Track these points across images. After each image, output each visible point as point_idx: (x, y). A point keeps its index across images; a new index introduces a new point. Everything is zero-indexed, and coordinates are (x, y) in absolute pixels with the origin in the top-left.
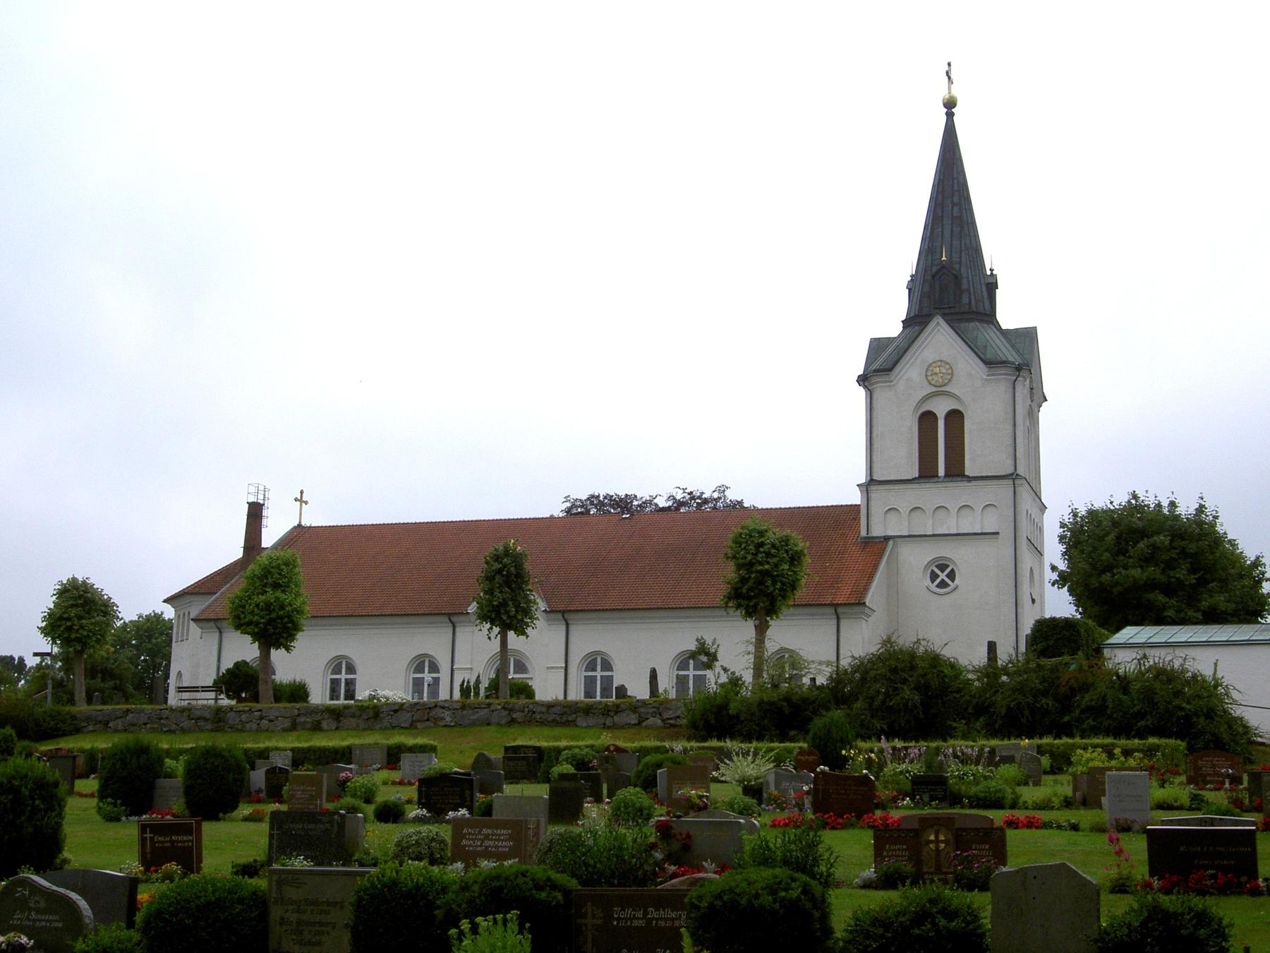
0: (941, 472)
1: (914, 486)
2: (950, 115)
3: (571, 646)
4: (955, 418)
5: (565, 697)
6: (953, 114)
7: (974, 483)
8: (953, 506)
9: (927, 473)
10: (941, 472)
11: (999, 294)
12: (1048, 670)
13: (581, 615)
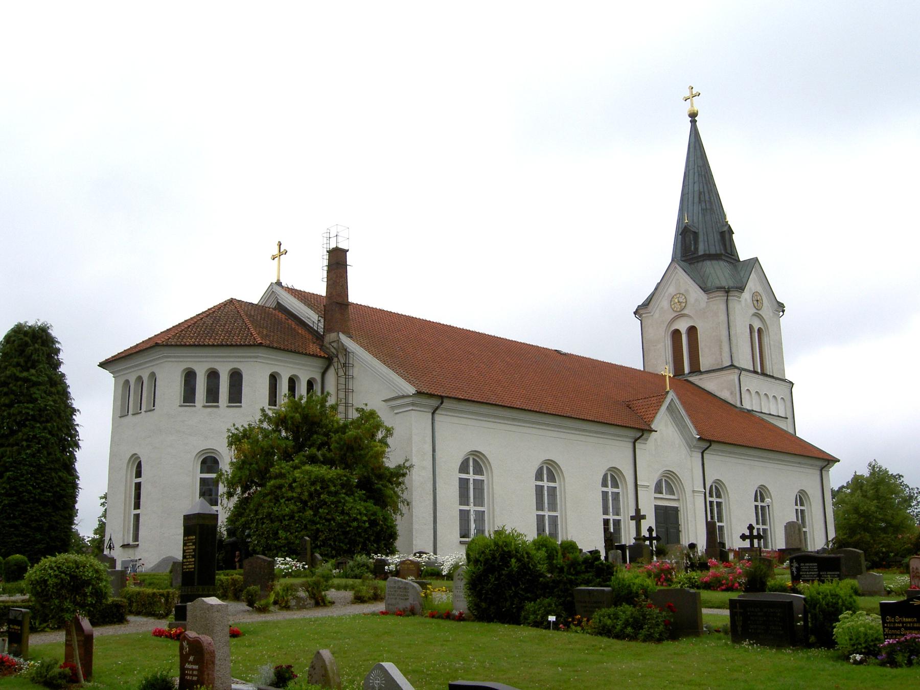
0: (687, 370)
2: (694, 122)
4: (692, 331)
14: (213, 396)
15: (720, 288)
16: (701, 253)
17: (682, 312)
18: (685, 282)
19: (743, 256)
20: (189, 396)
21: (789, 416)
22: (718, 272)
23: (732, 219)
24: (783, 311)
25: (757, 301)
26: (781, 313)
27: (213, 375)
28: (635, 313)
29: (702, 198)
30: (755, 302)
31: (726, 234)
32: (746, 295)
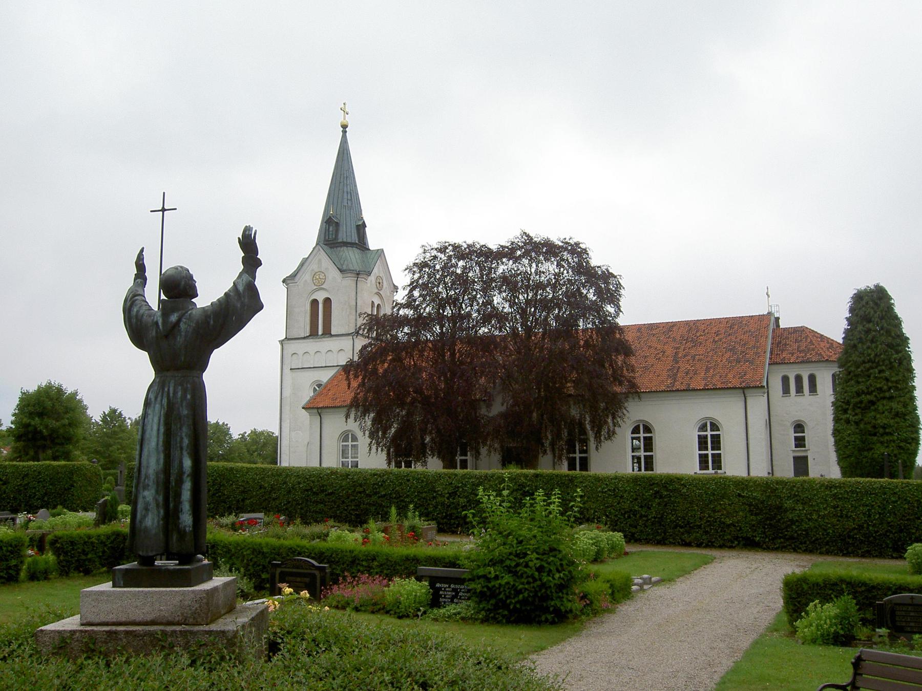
0: (320, 332)
1: (308, 340)
2: (344, 132)
3: (323, 432)
4: (328, 301)
5: (320, 465)
6: (346, 132)
7: (334, 338)
8: (301, 352)
9: (313, 334)
10: (320, 332)
11: (368, 230)
12: (488, 434)
13: (328, 410)
14: (799, 390)
15: (351, 271)
16: (340, 240)
17: (322, 287)
18: (325, 263)
19: (373, 244)
20: (786, 390)
21: (287, 370)
22: (352, 256)
23: (367, 216)
24: (397, 292)
25: (379, 284)
26: (395, 293)
27: (799, 379)
28: (284, 281)
29: (349, 196)
30: (378, 284)
31: (361, 228)
32: (372, 278)
